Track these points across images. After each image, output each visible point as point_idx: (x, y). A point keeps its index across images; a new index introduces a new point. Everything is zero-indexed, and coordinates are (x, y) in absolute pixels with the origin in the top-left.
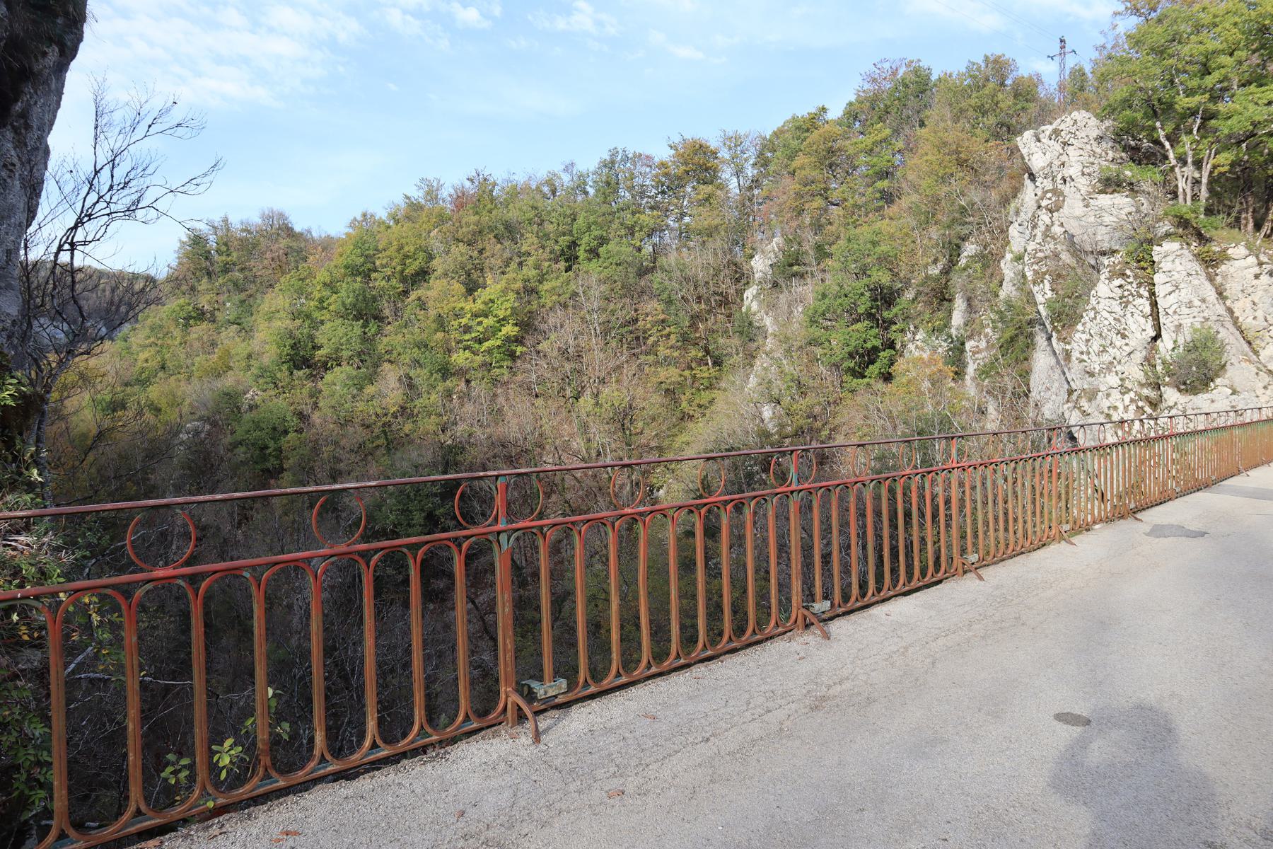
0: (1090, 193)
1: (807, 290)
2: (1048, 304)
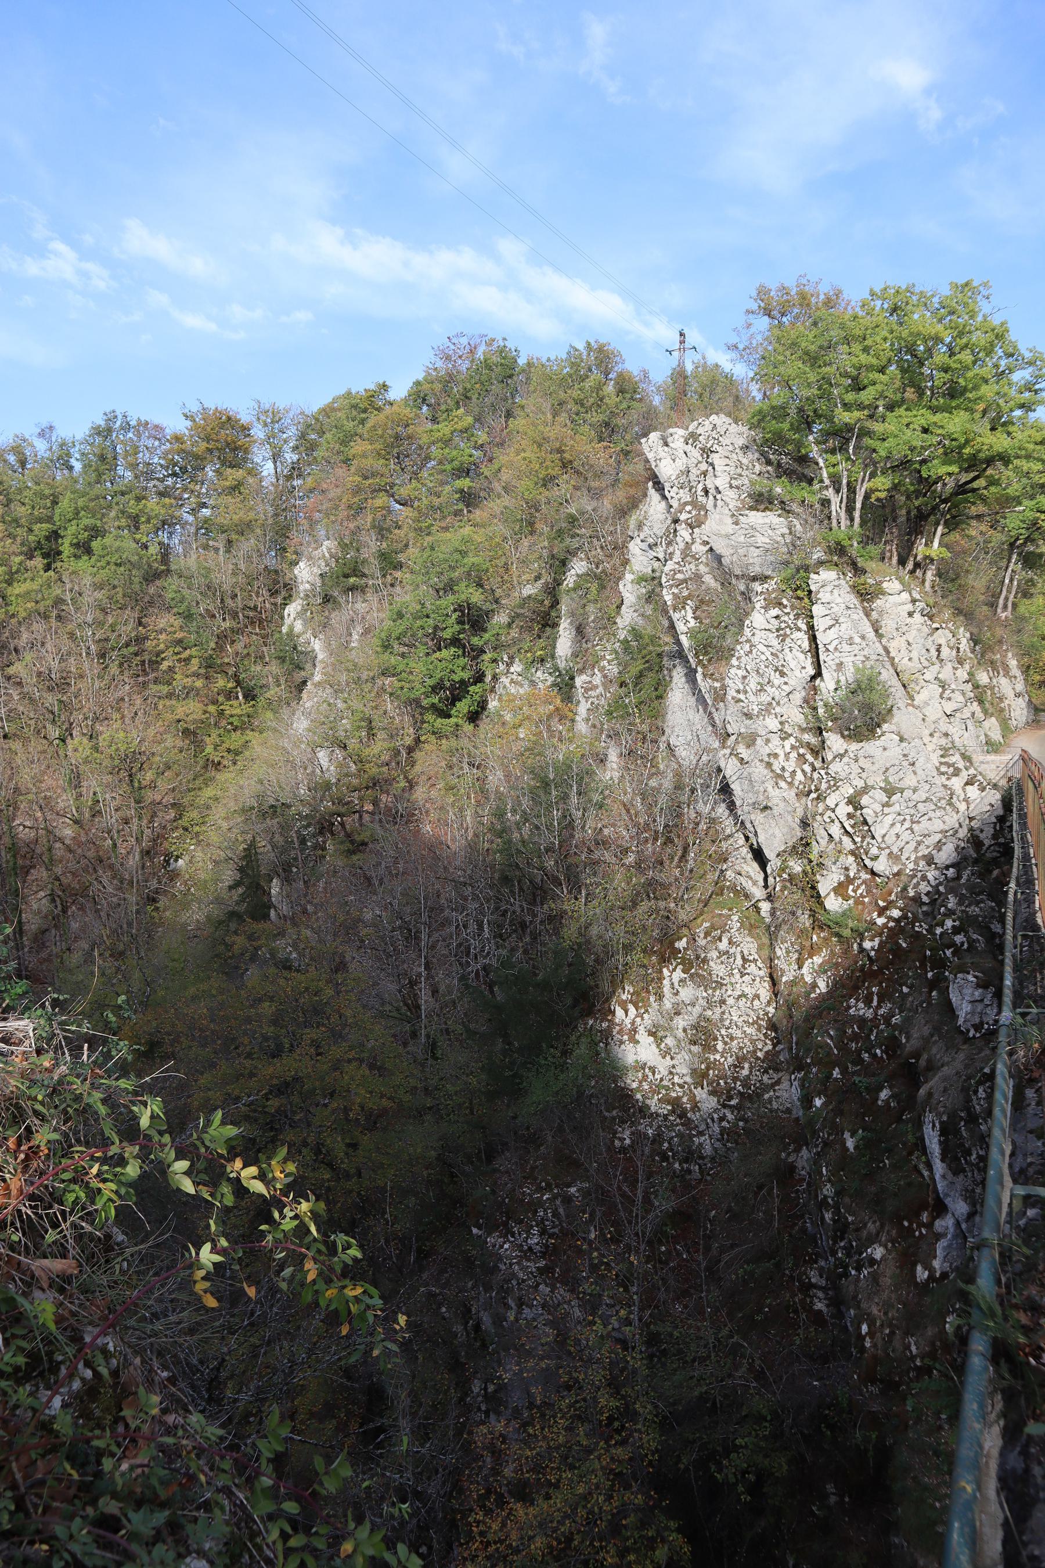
0: (739, 509)
1: (368, 610)
2: (692, 634)
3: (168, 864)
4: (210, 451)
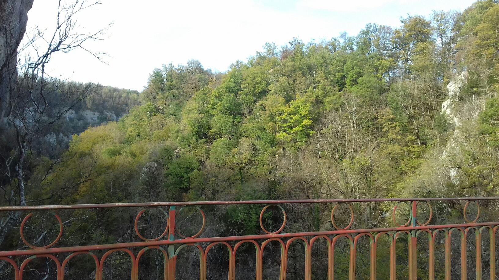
3: (382, 214)
4: (411, 36)
